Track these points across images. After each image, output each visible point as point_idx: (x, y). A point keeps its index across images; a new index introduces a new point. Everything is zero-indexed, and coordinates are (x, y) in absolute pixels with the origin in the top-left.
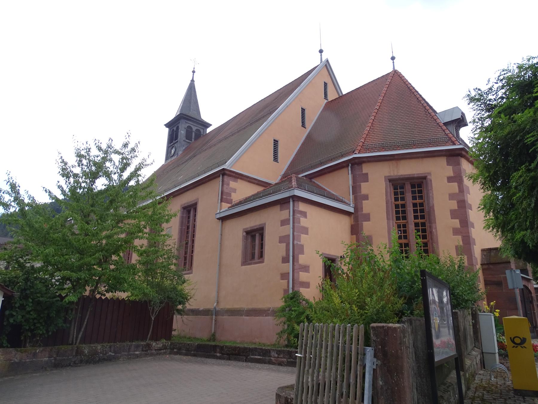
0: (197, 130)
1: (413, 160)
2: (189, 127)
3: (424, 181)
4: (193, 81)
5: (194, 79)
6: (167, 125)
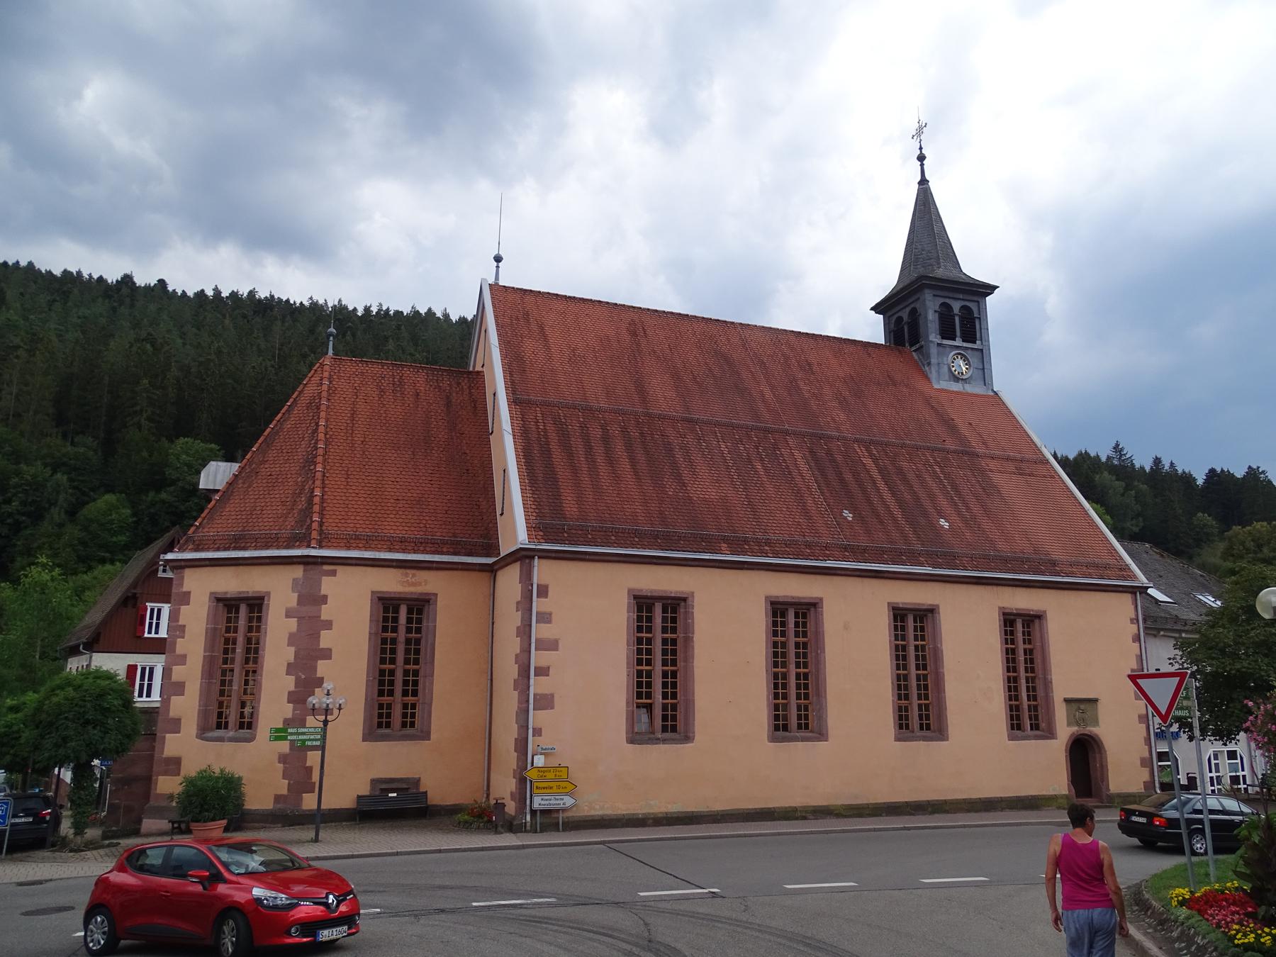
0: (963, 308)
1: (818, 577)
2: (943, 304)
3: (1037, 621)
4: (923, 182)
5: (927, 177)
6: (877, 309)
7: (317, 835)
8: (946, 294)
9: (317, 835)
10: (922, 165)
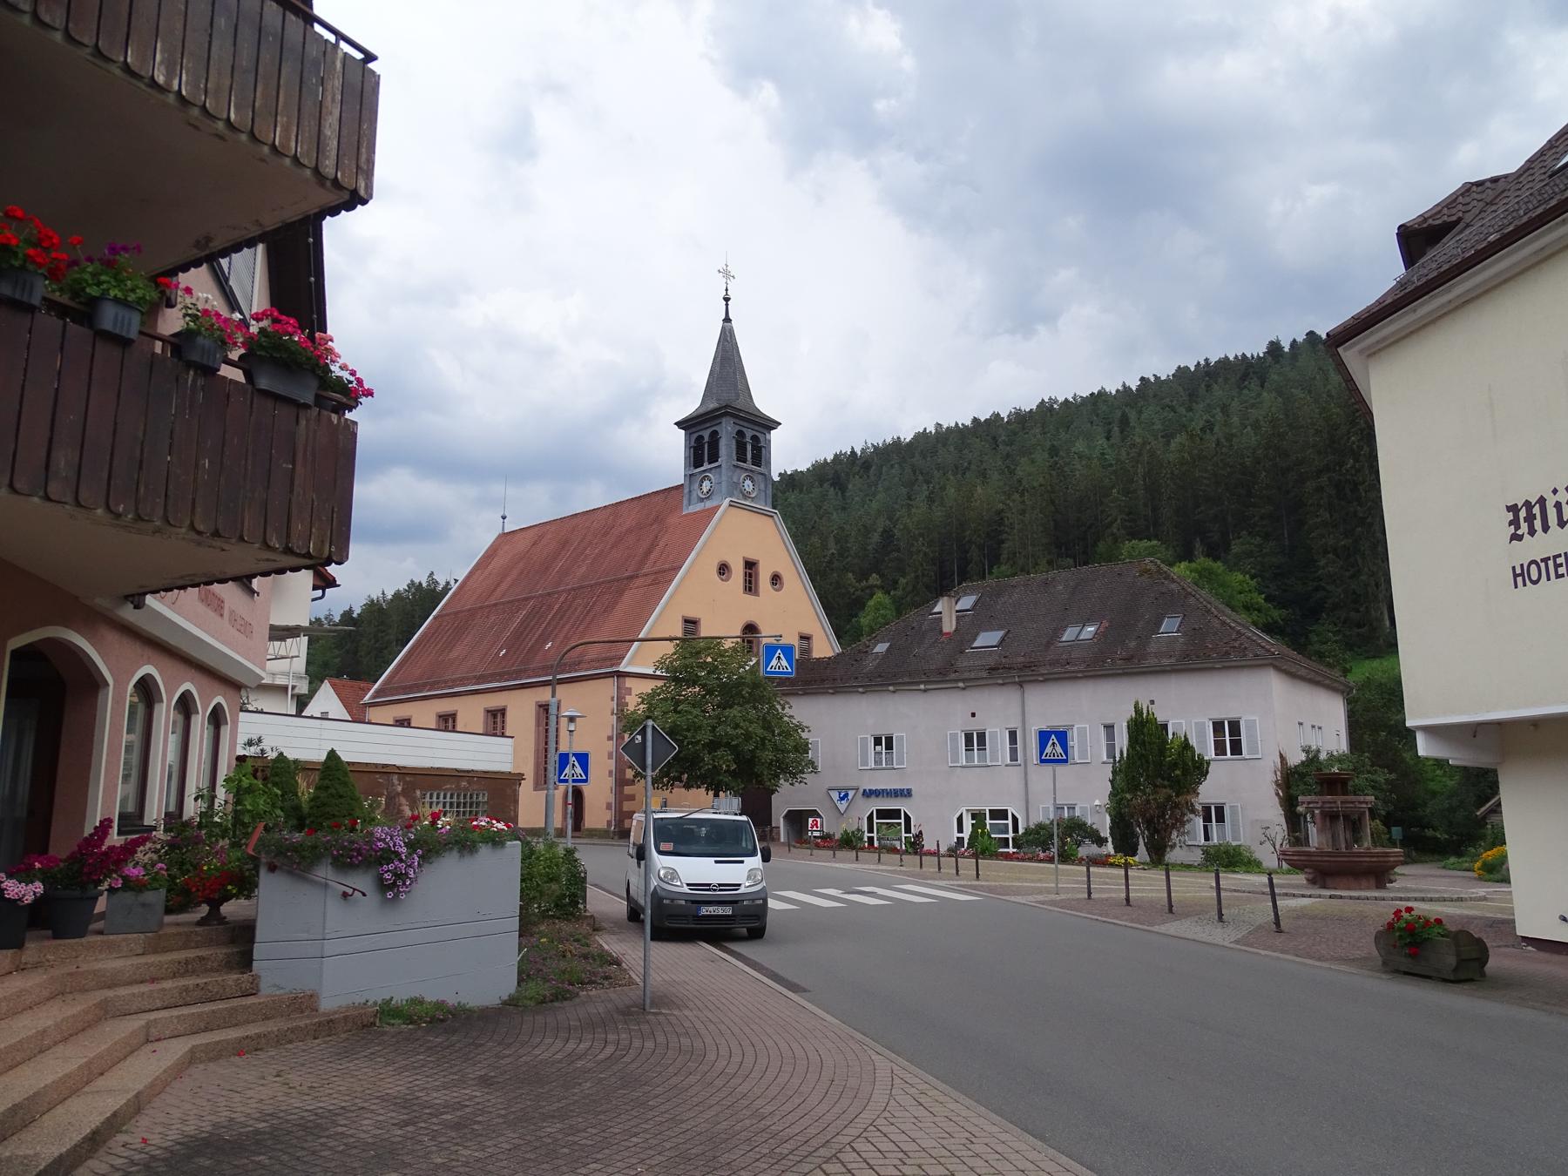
4: (727, 320)
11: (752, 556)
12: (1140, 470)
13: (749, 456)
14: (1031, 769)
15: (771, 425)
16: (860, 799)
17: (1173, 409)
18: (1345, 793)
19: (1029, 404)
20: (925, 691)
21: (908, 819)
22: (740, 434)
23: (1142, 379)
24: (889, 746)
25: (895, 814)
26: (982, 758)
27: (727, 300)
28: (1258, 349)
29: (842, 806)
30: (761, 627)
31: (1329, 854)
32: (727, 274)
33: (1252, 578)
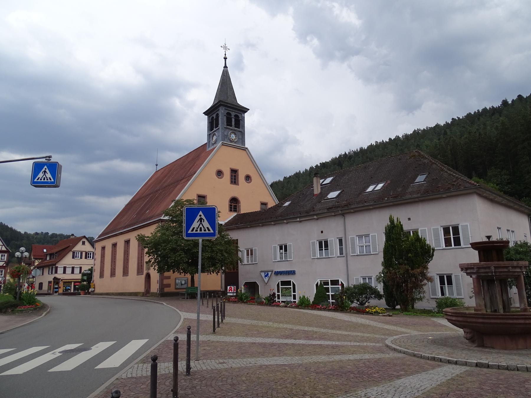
4: (226, 67)
6: (205, 113)
7: (154, 368)
8: (229, 109)
9: (154, 368)
10: (225, 61)
11: (235, 167)
12: (449, 147)
13: (233, 123)
14: (349, 258)
15: (245, 110)
16: (274, 277)
17: (464, 127)
18: (500, 259)
19: (410, 132)
20: (300, 222)
21: (294, 285)
22: (229, 114)
23: (453, 119)
24: (286, 250)
25: (288, 283)
26: (327, 254)
27: (225, 58)
28: (497, 104)
29: (266, 279)
30: (240, 199)
31: (483, 316)
32: (225, 48)
33: (497, 185)
